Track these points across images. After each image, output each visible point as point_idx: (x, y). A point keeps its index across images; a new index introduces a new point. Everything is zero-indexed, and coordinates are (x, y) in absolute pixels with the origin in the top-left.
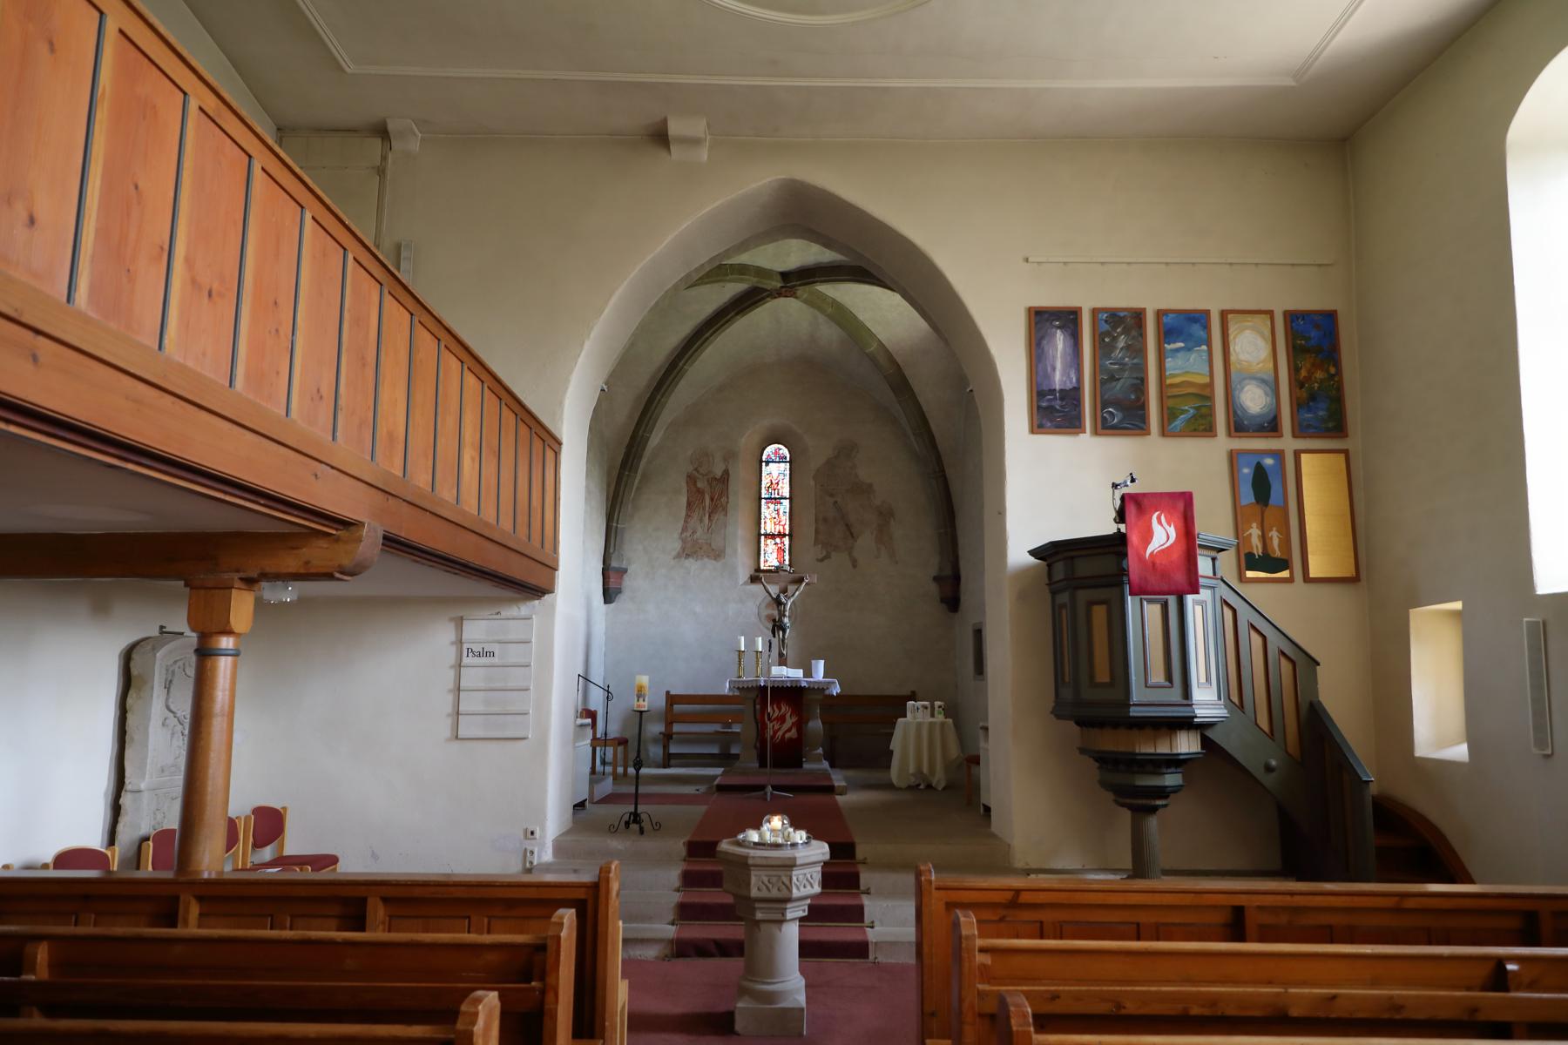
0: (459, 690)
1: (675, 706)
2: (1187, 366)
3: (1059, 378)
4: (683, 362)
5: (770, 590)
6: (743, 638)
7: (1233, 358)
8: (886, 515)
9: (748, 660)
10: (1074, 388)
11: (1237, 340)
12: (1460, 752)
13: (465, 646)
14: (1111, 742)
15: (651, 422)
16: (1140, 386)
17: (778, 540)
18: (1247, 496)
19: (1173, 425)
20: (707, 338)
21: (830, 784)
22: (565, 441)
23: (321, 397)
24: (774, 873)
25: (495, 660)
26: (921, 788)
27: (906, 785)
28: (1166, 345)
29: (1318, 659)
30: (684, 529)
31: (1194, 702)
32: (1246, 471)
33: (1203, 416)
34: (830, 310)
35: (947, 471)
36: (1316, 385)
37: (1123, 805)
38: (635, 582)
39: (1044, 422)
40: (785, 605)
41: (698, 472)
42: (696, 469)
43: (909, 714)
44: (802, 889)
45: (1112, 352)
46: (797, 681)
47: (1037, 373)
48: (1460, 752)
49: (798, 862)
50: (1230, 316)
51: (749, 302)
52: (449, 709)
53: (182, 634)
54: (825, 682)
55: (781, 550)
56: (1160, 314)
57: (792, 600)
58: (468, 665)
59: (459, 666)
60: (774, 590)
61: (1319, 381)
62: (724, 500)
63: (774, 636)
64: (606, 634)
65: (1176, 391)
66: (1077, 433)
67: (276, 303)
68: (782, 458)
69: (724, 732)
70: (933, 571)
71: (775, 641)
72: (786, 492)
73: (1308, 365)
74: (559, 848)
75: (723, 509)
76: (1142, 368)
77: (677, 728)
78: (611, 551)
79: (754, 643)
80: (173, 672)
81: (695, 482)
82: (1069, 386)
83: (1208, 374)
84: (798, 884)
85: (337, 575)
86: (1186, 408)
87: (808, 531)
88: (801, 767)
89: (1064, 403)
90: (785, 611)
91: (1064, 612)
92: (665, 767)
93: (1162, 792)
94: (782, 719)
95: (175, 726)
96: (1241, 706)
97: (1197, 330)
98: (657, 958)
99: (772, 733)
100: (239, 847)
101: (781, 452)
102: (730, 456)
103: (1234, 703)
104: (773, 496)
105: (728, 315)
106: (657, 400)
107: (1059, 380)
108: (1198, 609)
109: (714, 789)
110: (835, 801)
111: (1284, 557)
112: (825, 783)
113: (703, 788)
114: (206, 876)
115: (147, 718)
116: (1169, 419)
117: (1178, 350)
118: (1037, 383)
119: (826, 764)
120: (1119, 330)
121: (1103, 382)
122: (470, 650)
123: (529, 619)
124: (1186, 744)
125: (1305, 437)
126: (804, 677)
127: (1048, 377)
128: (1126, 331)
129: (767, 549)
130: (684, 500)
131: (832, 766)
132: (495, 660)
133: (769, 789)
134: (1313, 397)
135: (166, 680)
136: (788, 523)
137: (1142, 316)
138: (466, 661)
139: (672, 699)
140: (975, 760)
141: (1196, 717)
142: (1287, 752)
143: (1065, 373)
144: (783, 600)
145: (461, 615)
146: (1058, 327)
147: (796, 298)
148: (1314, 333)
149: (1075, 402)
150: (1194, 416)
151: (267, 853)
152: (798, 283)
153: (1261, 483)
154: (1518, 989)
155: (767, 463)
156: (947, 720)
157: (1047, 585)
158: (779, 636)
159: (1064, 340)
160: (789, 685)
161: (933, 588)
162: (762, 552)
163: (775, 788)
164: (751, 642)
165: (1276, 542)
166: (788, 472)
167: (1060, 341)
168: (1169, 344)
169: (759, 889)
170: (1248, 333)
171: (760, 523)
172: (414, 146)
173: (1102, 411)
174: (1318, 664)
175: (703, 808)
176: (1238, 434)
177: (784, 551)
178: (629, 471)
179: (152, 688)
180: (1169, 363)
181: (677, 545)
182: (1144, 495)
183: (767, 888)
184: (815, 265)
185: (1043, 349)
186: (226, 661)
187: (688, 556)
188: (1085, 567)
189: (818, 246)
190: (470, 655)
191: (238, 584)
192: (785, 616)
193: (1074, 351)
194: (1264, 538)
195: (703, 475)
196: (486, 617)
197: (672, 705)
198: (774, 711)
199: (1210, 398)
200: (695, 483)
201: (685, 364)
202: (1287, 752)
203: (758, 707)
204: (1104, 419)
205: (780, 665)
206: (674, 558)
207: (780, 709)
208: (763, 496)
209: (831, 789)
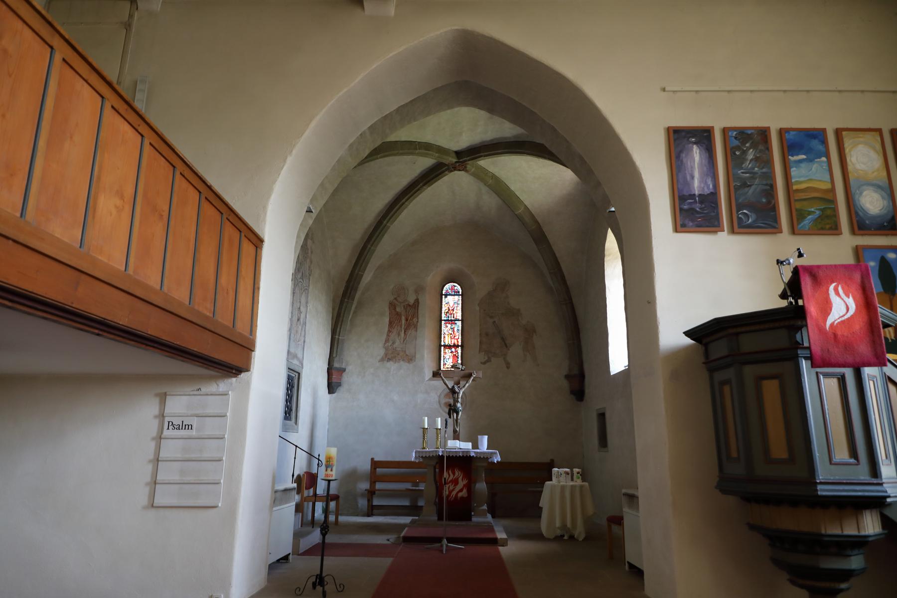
0: (158, 460)
1: (377, 469)
3: (697, 185)
6: (426, 418)
8: (530, 331)
9: (430, 435)
10: (712, 193)
11: (852, 153)
13: (167, 419)
16: (770, 191)
17: (453, 350)
19: (802, 224)
20: (403, 204)
21: (495, 537)
22: (266, 239)
25: (193, 433)
26: (565, 538)
27: (553, 537)
28: (790, 157)
30: (387, 341)
31: (884, 481)
33: (828, 217)
35: (573, 300)
37: (802, 586)
38: (350, 379)
39: (686, 222)
40: (458, 393)
41: (397, 300)
42: (395, 299)
43: (554, 478)
45: (743, 163)
46: (467, 452)
47: (678, 181)
50: (844, 133)
52: (148, 478)
54: (488, 453)
55: (455, 357)
56: (782, 132)
57: (463, 390)
58: (167, 437)
59: (159, 438)
60: (450, 384)
62: (415, 320)
63: (450, 417)
64: (329, 416)
66: (715, 232)
68: (457, 292)
69: (412, 490)
70: (565, 371)
71: (450, 421)
72: (459, 315)
75: (414, 327)
76: (770, 177)
77: (378, 486)
78: (334, 355)
79: (435, 422)
82: (707, 192)
83: (829, 181)
86: (813, 210)
87: (475, 342)
88: (471, 520)
89: (703, 206)
90: (458, 398)
91: (727, 389)
92: (368, 516)
93: (847, 575)
94: (455, 482)
97: (816, 144)
99: (447, 493)
101: (456, 288)
102: (419, 289)
104: (450, 319)
105: (417, 186)
106: (368, 248)
107: (698, 187)
109: (401, 540)
110: (498, 552)
112: (491, 536)
113: (392, 538)
116: (798, 220)
117: (801, 161)
118: (678, 188)
119: (489, 516)
120: (748, 145)
121: (737, 189)
122: (171, 424)
123: (226, 395)
124: (871, 525)
126: (473, 449)
127: (688, 184)
128: (754, 146)
129: (446, 356)
130: (387, 320)
131: (493, 517)
132: (193, 433)
133: (445, 541)
136: (460, 338)
138: (166, 433)
140: (618, 520)
141: (889, 497)
143: (703, 180)
144: (457, 390)
146: (695, 143)
147: (466, 171)
149: (714, 205)
150: (820, 217)
152: (468, 158)
155: (446, 296)
156: (584, 483)
157: (704, 363)
158: (454, 416)
159: (700, 153)
160: (461, 455)
161: (565, 384)
162: (442, 358)
164: (432, 422)
166: (460, 302)
167: (696, 155)
168: (792, 156)
170: (861, 147)
171: (441, 338)
173: (738, 211)
175: (389, 561)
176: (862, 232)
177: (458, 358)
178: (348, 299)
180: (794, 172)
181: (382, 352)
182: (818, 267)
184: (480, 143)
185: (682, 161)
187: (389, 360)
188: (750, 343)
189: (484, 112)
190: (171, 427)
192: (458, 402)
193: (709, 162)
196: (187, 393)
197: (375, 469)
198: (449, 475)
199: (833, 201)
200: (395, 309)
203: (437, 470)
204: (739, 219)
205: (454, 439)
206: (379, 362)
207: (454, 474)
208: (443, 319)
209: (494, 541)
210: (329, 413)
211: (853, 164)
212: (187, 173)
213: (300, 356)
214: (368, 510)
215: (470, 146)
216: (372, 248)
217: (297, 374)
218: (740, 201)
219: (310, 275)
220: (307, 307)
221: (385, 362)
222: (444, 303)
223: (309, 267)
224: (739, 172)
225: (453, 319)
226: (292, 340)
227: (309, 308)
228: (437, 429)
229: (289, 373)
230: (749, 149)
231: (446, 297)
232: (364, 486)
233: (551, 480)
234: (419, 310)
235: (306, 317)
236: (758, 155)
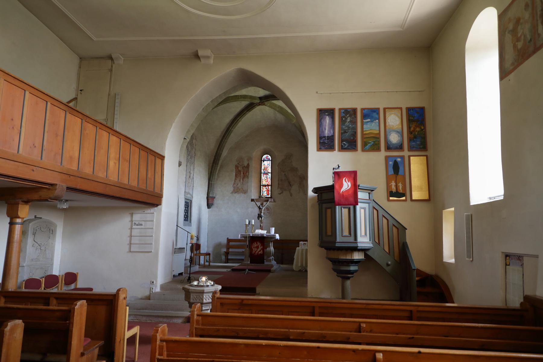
1: (230, 243)
2: (371, 127)
3: (327, 132)
4: (231, 128)
5: (257, 204)
6: (253, 220)
7: (387, 124)
10: (332, 135)
11: (389, 118)
12: (453, 261)
13: (133, 222)
14: (335, 255)
15: (222, 148)
16: (355, 134)
17: (267, 187)
18: (391, 172)
19: (365, 148)
20: (238, 120)
22: (166, 156)
23: (35, 147)
24: (198, 295)
25: (143, 227)
28: (364, 120)
29: (406, 228)
30: (234, 184)
31: (358, 242)
32: (391, 163)
33: (376, 144)
34: (278, 109)
36: (417, 133)
38: (218, 201)
40: (262, 209)
42: (238, 164)
44: (207, 300)
48: (453, 261)
49: (205, 291)
50: (386, 110)
51: (251, 107)
53: (41, 218)
55: (268, 191)
56: (362, 110)
61: (417, 131)
62: (247, 173)
64: (208, 219)
65: (367, 136)
66: (333, 151)
67: (12, 120)
73: (414, 126)
74: (162, 287)
75: (247, 177)
78: (210, 191)
80: (36, 230)
81: (238, 167)
82: (330, 135)
84: (206, 298)
85: (50, 200)
86: (370, 142)
88: (264, 263)
90: (262, 211)
94: (258, 247)
95: (37, 246)
96: (379, 243)
97: (375, 115)
98: (181, 323)
100: (59, 285)
101: (268, 157)
102: (250, 159)
103: (376, 242)
104: (265, 172)
108: (363, 211)
111: (404, 193)
114: (10, 290)
115: (26, 244)
117: (368, 122)
118: (319, 134)
120: (348, 116)
124: (357, 256)
125: (412, 151)
127: (323, 132)
128: (350, 116)
130: (234, 174)
132: (143, 227)
134: (415, 137)
135: (33, 232)
136: (270, 181)
137: (356, 111)
138: (134, 227)
139: (229, 240)
141: (358, 247)
142: (395, 260)
143: (329, 131)
144: (261, 207)
145: (132, 212)
146: (327, 115)
147: (266, 105)
148: (416, 115)
149: (332, 140)
150: (373, 145)
151: (73, 286)
152: (265, 100)
153: (396, 167)
154: (364, 332)
155: (264, 161)
159: (329, 119)
160: (260, 236)
163: (249, 270)
165: (401, 187)
166: (270, 164)
167: (327, 120)
168: (365, 120)
169: (193, 300)
172: (121, 62)
174: (406, 229)
177: (269, 191)
179: (28, 235)
180: (365, 126)
181: (232, 189)
183: (196, 299)
185: (322, 123)
186: (18, 226)
187: (235, 193)
191: (21, 203)
192: (262, 213)
193: (332, 123)
194: (396, 186)
195: (240, 165)
197: (229, 242)
199: (379, 138)
201: (232, 128)
202: (395, 260)
207: (257, 244)
208: (262, 172)
210: (208, 217)
211: (388, 123)
212: (135, 144)
213: (191, 193)
214: (225, 260)
215: (264, 95)
216: (225, 140)
217: (190, 201)
218: (343, 138)
219: (195, 156)
220: (194, 170)
221: (234, 194)
222: (262, 165)
223: (194, 152)
224: (344, 127)
225: (267, 172)
226: (186, 187)
227: (195, 171)
228: (252, 225)
229: (186, 201)
230: (348, 117)
231: (263, 162)
232: (225, 250)
233: (299, 247)
234: (249, 169)
235: (194, 175)
236: (351, 120)
